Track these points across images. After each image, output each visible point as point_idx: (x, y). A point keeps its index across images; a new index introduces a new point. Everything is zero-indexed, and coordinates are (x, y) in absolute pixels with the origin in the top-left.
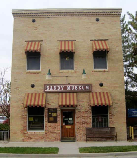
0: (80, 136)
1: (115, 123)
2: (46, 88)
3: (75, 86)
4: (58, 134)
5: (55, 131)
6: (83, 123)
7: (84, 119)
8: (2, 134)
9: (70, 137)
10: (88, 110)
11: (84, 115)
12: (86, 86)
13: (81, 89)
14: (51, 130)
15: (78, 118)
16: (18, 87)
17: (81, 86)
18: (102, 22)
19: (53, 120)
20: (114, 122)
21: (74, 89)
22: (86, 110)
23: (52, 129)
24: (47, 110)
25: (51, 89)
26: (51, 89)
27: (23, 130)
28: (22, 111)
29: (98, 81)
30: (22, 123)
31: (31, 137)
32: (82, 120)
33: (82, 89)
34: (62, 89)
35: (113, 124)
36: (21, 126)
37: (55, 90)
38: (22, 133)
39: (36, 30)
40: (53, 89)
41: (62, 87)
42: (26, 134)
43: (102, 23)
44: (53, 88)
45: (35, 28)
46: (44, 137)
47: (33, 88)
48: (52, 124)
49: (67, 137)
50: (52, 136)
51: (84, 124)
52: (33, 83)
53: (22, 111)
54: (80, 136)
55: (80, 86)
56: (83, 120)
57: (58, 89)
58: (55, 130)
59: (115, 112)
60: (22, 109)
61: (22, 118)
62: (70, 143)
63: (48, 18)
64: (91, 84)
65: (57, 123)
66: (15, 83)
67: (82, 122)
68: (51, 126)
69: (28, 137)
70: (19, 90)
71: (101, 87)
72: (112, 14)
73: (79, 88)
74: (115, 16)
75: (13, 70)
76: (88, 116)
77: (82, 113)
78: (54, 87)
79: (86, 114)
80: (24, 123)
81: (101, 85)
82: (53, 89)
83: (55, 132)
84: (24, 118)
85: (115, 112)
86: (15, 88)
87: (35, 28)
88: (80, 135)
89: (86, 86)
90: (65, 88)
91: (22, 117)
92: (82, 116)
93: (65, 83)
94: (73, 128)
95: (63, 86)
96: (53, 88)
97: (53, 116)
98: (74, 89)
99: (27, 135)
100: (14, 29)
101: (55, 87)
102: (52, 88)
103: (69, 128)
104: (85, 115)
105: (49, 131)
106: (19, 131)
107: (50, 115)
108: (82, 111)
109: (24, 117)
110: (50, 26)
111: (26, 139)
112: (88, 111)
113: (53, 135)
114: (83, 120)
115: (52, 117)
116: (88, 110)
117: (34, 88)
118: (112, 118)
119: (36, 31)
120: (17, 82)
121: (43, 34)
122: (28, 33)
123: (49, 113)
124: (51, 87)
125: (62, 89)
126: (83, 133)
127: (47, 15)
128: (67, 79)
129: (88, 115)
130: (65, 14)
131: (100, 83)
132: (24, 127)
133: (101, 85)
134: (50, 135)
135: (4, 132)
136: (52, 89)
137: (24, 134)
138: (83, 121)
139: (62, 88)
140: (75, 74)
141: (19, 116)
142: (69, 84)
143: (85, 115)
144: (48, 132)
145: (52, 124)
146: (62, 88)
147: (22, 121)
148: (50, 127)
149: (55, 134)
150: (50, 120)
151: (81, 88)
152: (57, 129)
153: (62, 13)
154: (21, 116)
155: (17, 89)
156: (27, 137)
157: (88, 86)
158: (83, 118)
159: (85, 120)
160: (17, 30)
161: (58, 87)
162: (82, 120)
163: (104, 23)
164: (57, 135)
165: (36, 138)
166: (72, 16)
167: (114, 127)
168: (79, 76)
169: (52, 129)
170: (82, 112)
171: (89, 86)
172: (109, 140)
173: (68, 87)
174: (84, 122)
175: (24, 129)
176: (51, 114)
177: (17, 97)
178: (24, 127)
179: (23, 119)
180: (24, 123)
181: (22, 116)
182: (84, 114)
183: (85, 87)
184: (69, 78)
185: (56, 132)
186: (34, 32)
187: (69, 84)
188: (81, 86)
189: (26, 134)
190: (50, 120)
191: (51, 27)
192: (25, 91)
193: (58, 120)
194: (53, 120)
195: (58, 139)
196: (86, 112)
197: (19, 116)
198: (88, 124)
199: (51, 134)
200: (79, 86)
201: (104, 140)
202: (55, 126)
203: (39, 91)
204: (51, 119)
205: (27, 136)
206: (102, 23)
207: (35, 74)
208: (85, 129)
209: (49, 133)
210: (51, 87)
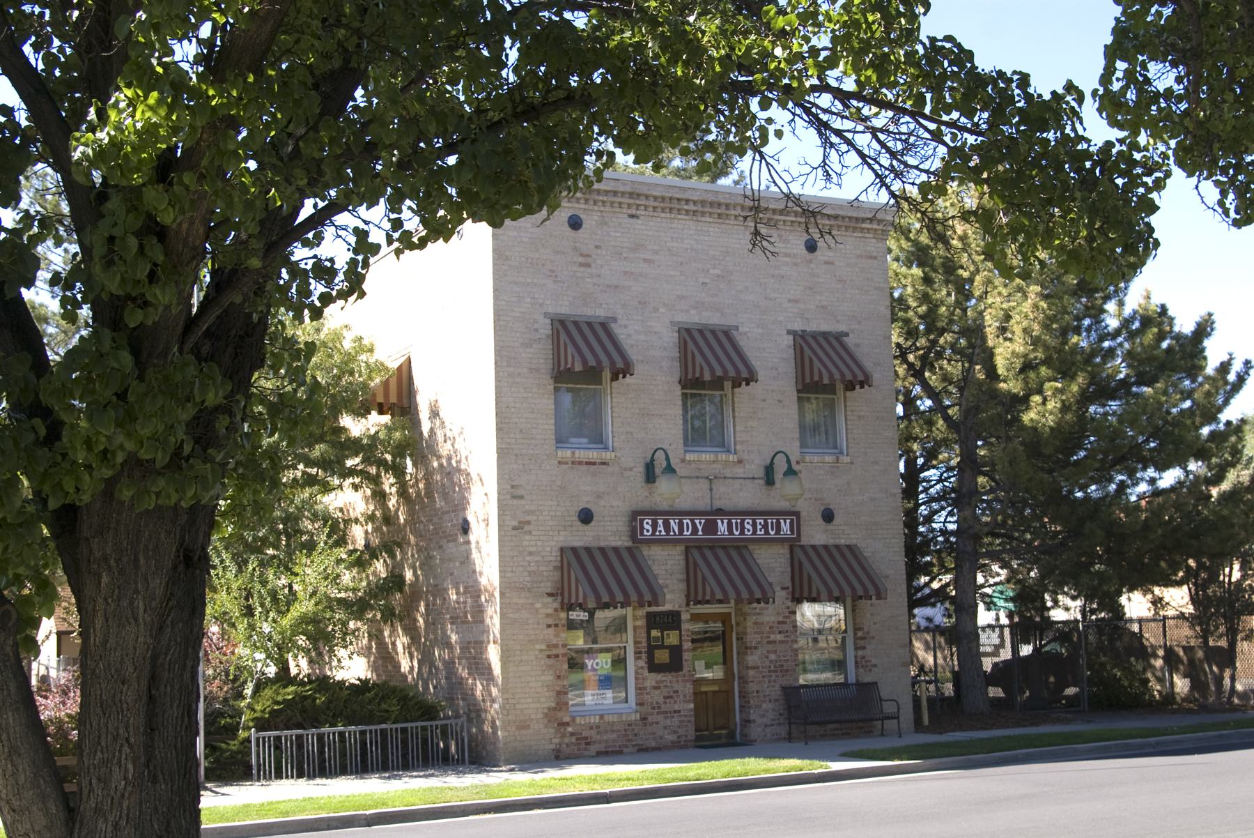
0: (764, 720)
1: (875, 666)
2: (642, 528)
3: (743, 521)
4: (686, 716)
5: (676, 708)
6: (772, 668)
7: (775, 652)
8: (330, 758)
9: (716, 729)
10: (787, 617)
11: (772, 637)
12: (782, 521)
13: (763, 532)
14: (661, 700)
15: (756, 648)
16: (529, 523)
17: (765, 521)
18: (826, 259)
19: (668, 661)
20: (874, 661)
21: (742, 533)
22: (781, 619)
23: (666, 698)
24: (644, 620)
25: (660, 531)
26: (660, 531)
27: (554, 709)
28: (549, 626)
29: (816, 500)
30: (549, 677)
31: (586, 738)
32: (767, 657)
33: (767, 532)
34: (700, 533)
35: (870, 670)
36: (547, 694)
37: (675, 534)
38: (549, 721)
39: (588, 265)
40: (668, 534)
41: (700, 523)
42: (568, 724)
43: (827, 263)
44: (667, 525)
45: (581, 260)
46: (636, 735)
47: (586, 527)
48: (664, 678)
49: (707, 730)
50: (665, 728)
51: (774, 674)
52: (588, 502)
53: (549, 626)
54: (764, 720)
55: (760, 521)
56: (773, 657)
57: (685, 533)
58: (675, 702)
59: (875, 623)
60: (548, 615)
61: (549, 657)
62: (714, 750)
63: (632, 216)
64: (797, 514)
65: (682, 670)
66: (515, 502)
67: (767, 663)
68: (659, 688)
69: (577, 739)
70: (534, 533)
71: (830, 527)
72: (864, 225)
73: (759, 527)
74: (871, 235)
75: (504, 446)
76: (787, 642)
77: (767, 629)
78: (672, 521)
79: (780, 632)
80: (559, 677)
81: (828, 516)
82: (668, 534)
83: (675, 712)
84: (557, 656)
85: (875, 623)
86: (515, 523)
87: (581, 260)
88: (763, 716)
89: (719, 521)
90: (711, 527)
91: (550, 653)
92: (769, 642)
93: (703, 505)
94: (726, 692)
95: (703, 521)
96: (667, 525)
97: (667, 642)
98: (742, 533)
99: (570, 729)
100: (494, 251)
101: (674, 525)
102: (662, 528)
103: (714, 692)
104: (779, 637)
105: (654, 708)
106: (540, 716)
107: (656, 639)
108: (766, 619)
109: (555, 652)
110: (642, 256)
111: (567, 745)
112: (788, 620)
113: (668, 722)
114: (773, 657)
115: (662, 647)
116: (787, 617)
117: (592, 524)
118: (864, 648)
119: (589, 270)
120: (522, 497)
121: (616, 287)
122: (556, 276)
123: (655, 633)
124: (660, 522)
125: (700, 533)
126: (774, 710)
127: (629, 206)
128: (711, 490)
129: (787, 636)
130: (699, 208)
131: (822, 508)
132: (559, 693)
133: (828, 516)
134: (657, 723)
135: (446, 725)
136: (663, 533)
137: (559, 724)
138: (771, 661)
139: (700, 528)
140: (739, 471)
141: (538, 647)
142: (720, 512)
143: (779, 637)
144: (650, 711)
145: (664, 678)
146: (700, 528)
147: (551, 672)
148: (657, 692)
149: (676, 721)
150: (656, 662)
151: (765, 526)
152: (681, 697)
153: (687, 201)
154: (543, 647)
155: (526, 528)
156: (573, 740)
157: (788, 521)
158: (771, 647)
159: (779, 656)
160: (507, 259)
161: (685, 521)
162: (767, 657)
163: (832, 263)
164: (681, 722)
165: (606, 741)
166: (720, 221)
167: (876, 683)
168: (753, 478)
169: (666, 698)
170: (768, 623)
171: (792, 520)
172: (814, 738)
173: (719, 521)
174: (775, 667)
175: (557, 704)
176: (659, 634)
177: (526, 564)
178: (559, 693)
179: (551, 661)
180: (559, 677)
181: (548, 646)
182: (773, 633)
183: (778, 524)
184: (721, 488)
185: (679, 711)
186: (579, 275)
187: (721, 509)
188: (765, 521)
189: (568, 724)
190: (656, 662)
191: (645, 260)
192: (555, 538)
193: (686, 660)
194: (668, 661)
195: (686, 736)
196: (779, 623)
197: (538, 647)
198: (787, 671)
199: (660, 718)
200: (758, 521)
201: (843, 734)
202: (676, 687)
203: (613, 538)
204: (662, 656)
205: (572, 734)
206: (827, 263)
207: (594, 464)
208: (779, 693)
209: (652, 714)
210: (660, 522)
